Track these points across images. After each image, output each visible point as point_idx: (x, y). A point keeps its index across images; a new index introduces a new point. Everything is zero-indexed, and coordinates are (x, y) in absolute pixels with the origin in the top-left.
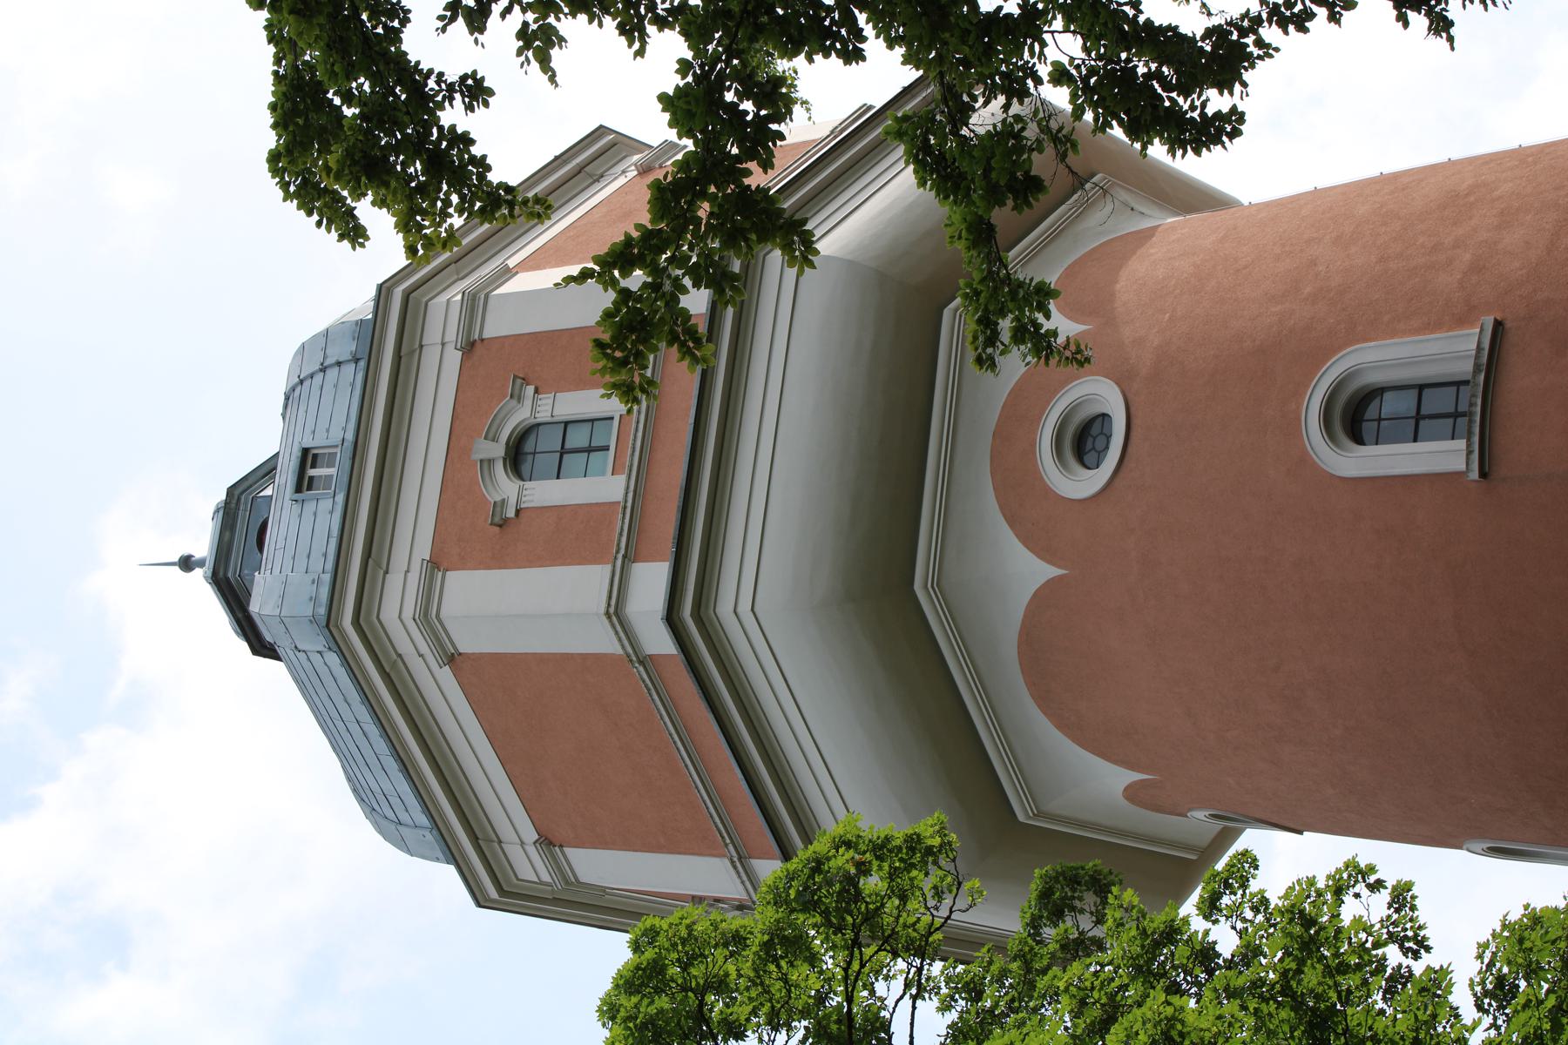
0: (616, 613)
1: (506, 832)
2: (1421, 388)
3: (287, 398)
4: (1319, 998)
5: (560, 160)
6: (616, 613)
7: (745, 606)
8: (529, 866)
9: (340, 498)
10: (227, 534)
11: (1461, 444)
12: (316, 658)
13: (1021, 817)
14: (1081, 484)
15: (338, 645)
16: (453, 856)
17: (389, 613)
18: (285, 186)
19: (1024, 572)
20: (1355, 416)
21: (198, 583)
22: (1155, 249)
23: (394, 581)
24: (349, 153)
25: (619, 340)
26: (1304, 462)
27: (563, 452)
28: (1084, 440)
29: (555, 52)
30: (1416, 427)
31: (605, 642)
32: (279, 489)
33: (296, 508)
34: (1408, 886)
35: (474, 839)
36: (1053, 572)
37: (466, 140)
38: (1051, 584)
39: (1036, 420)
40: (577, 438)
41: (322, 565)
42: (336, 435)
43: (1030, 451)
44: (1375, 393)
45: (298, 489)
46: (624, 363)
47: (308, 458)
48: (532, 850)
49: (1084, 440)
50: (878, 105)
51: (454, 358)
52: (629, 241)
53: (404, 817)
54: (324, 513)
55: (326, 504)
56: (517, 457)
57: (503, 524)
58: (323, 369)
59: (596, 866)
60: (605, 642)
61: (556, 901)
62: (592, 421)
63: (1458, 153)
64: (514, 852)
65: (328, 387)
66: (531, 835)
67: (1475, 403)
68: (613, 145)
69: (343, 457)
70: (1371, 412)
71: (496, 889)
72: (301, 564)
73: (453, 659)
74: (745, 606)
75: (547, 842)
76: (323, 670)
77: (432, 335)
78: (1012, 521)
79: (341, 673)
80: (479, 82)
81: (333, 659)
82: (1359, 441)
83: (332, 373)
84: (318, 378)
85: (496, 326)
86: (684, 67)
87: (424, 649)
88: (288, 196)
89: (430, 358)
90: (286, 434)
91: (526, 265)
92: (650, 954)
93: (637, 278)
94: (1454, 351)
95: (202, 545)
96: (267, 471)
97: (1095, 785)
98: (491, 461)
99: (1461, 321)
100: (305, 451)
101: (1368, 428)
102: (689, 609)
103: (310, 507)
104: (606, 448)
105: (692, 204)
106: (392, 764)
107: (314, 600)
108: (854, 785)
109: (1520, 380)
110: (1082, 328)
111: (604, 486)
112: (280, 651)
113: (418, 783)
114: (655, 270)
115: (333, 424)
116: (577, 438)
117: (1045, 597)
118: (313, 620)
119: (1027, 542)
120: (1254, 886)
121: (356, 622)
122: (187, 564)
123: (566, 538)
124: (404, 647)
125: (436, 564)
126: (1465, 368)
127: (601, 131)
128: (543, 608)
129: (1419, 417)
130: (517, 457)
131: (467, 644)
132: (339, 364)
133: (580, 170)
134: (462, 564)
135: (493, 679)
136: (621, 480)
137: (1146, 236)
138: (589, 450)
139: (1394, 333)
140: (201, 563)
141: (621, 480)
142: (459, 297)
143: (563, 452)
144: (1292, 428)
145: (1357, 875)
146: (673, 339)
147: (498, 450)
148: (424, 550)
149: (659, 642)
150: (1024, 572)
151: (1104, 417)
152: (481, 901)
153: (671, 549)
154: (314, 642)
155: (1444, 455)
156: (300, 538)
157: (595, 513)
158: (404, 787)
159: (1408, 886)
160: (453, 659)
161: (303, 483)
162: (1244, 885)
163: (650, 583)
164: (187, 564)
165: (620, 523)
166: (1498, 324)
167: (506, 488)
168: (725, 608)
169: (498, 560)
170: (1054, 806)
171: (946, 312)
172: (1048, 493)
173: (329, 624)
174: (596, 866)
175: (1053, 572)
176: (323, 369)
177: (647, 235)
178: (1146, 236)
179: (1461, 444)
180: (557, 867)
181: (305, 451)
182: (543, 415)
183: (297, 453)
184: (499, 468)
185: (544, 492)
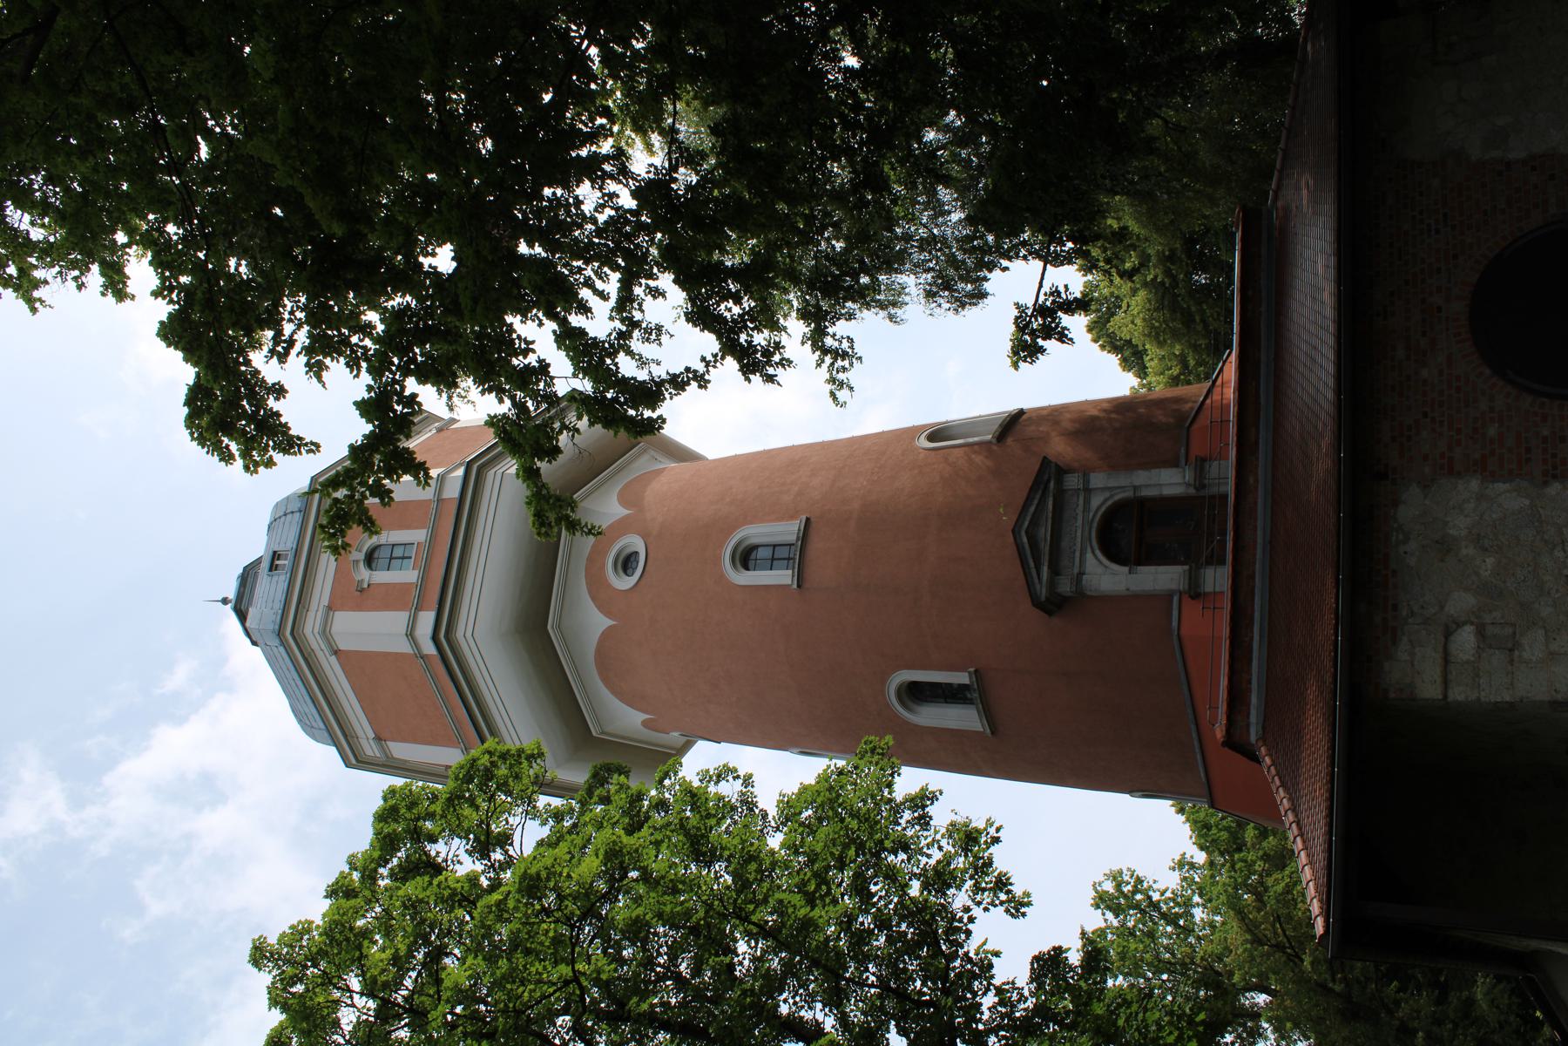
0: (411, 634)
1: (360, 733)
2: (774, 546)
4: (699, 829)
8: (370, 749)
11: (790, 572)
14: (624, 583)
15: (283, 643)
17: (308, 630)
18: (192, 434)
19: (595, 622)
20: (745, 557)
22: (663, 478)
23: (311, 614)
24: (213, 419)
25: (331, 523)
26: (722, 577)
27: (391, 558)
28: (627, 563)
29: (324, 374)
30: (772, 563)
31: (405, 647)
34: (750, 776)
35: (345, 736)
36: (611, 623)
37: (278, 415)
39: (605, 553)
40: (398, 552)
41: (278, 606)
43: (604, 565)
44: (755, 547)
46: (334, 535)
47: (276, 555)
49: (627, 563)
52: (338, 474)
54: (281, 580)
55: (283, 578)
56: (370, 560)
57: (362, 590)
59: (401, 750)
60: (405, 647)
63: (1045, 404)
64: (364, 742)
67: (797, 554)
69: (291, 556)
70: (753, 556)
73: (336, 652)
75: (379, 739)
78: (593, 599)
80: (282, 387)
81: (282, 649)
82: (747, 569)
86: (370, 388)
88: (193, 439)
90: (268, 545)
92: (392, 802)
93: (341, 493)
94: (788, 530)
95: (232, 595)
97: (627, 719)
99: (792, 517)
101: (751, 564)
102: (444, 634)
105: (371, 456)
106: (307, 698)
108: (519, 720)
109: (816, 545)
111: (407, 575)
113: (322, 712)
114: (352, 489)
115: (287, 543)
116: (398, 552)
117: (607, 635)
120: (681, 775)
122: (225, 601)
123: (389, 598)
124: (315, 646)
125: (330, 608)
126: (792, 538)
128: (379, 631)
129: (773, 559)
134: (342, 609)
135: (356, 663)
136: (416, 572)
137: (660, 472)
139: (762, 521)
141: (416, 572)
142: (460, 472)
143: (391, 558)
144: (717, 560)
145: (724, 773)
146: (360, 522)
147: (361, 556)
149: (429, 649)
150: (595, 622)
151: (636, 553)
155: (782, 576)
156: (270, 591)
157: (403, 588)
158: (314, 711)
159: (750, 776)
160: (336, 652)
161: (273, 567)
162: (676, 774)
163: (427, 619)
164: (225, 601)
165: (415, 593)
166: (808, 519)
167: (364, 574)
168: (459, 634)
169: (359, 607)
170: (608, 729)
172: (609, 586)
173: (280, 633)
174: (401, 750)
175: (611, 623)
177: (347, 470)
178: (660, 472)
179: (790, 572)
180: (383, 749)
184: (361, 565)
185: (381, 577)
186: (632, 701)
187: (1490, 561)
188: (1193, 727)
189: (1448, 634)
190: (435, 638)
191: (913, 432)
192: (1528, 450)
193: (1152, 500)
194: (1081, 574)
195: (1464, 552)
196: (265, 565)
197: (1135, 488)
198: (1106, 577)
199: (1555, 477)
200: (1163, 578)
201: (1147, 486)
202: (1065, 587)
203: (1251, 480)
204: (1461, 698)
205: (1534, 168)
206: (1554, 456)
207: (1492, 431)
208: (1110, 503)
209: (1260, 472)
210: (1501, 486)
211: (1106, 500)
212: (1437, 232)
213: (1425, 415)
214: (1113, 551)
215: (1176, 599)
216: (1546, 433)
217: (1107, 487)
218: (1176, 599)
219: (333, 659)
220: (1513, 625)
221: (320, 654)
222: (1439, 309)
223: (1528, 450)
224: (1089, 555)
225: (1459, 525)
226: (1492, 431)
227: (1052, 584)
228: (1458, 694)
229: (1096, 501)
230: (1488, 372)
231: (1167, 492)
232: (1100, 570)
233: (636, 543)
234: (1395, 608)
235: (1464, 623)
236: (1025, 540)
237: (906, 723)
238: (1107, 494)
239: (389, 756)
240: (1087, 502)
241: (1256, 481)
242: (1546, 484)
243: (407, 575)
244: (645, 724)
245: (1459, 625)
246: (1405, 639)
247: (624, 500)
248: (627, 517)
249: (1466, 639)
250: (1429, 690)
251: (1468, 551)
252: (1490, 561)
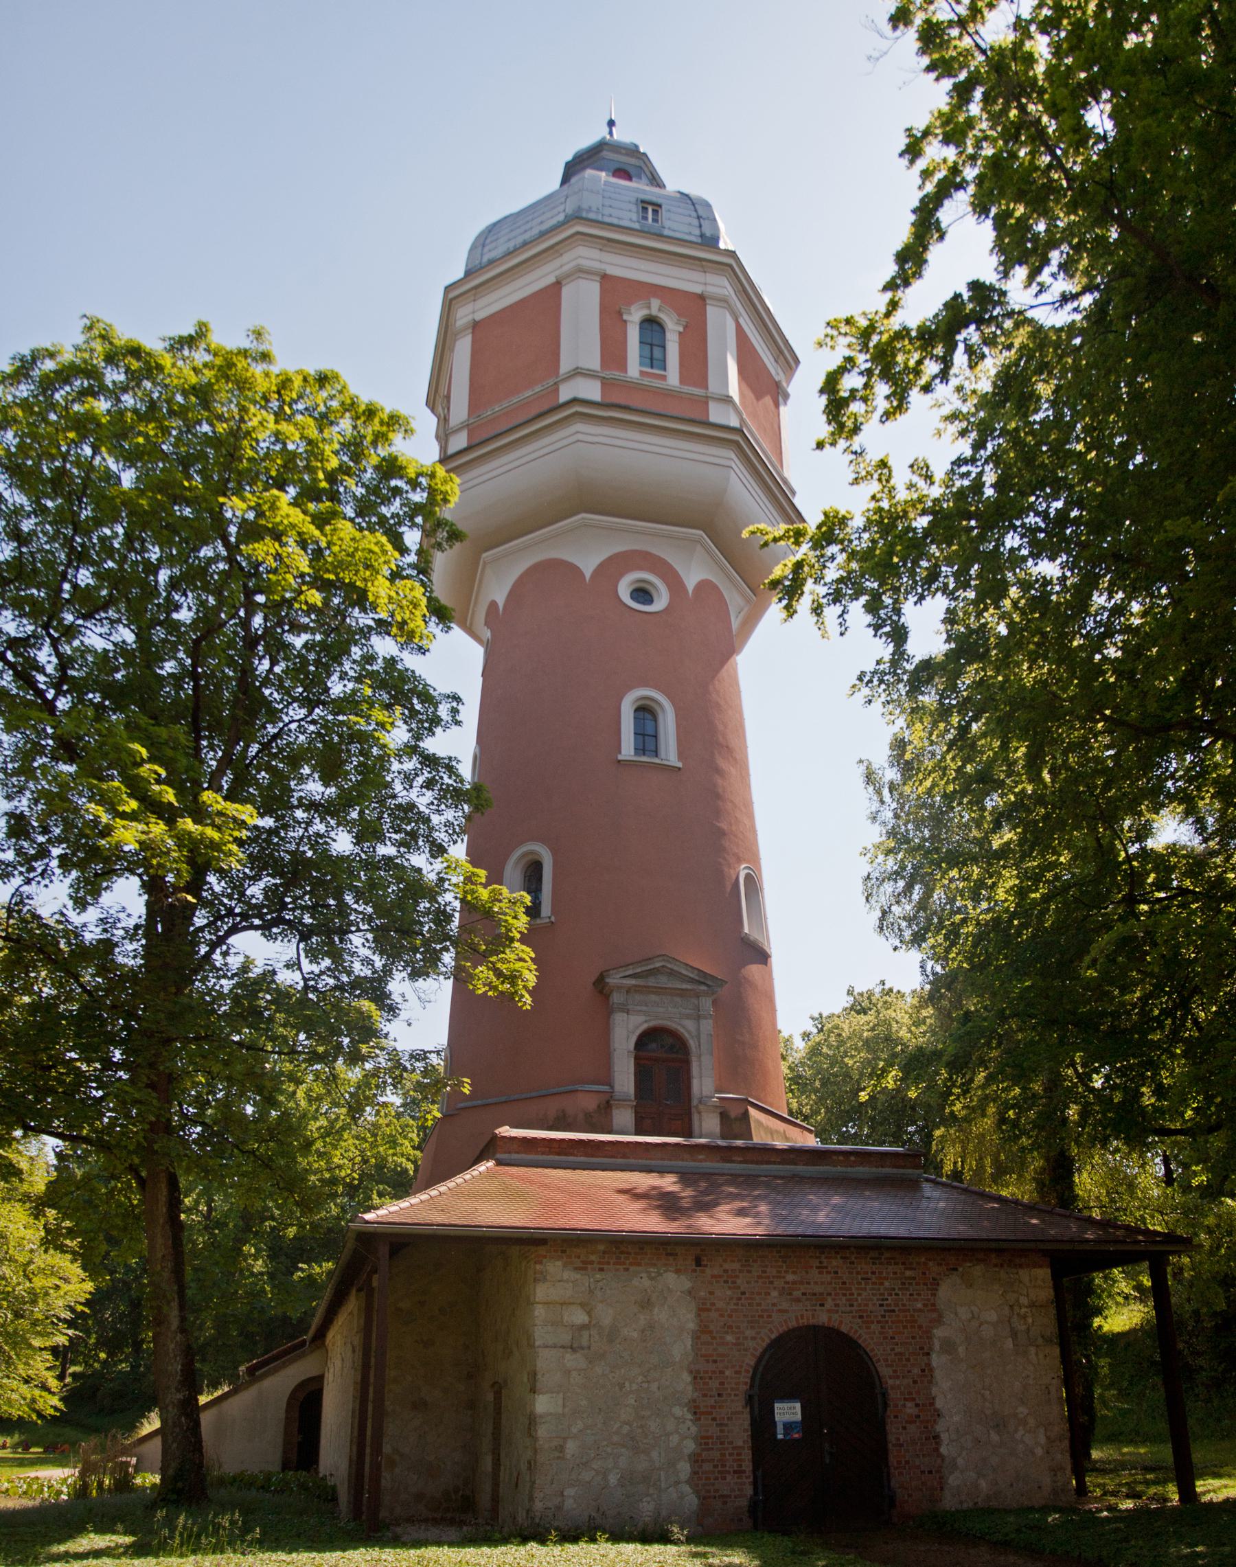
0: (578, 373)
1: (481, 303)
2: (656, 736)
3: (687, 195)
5: (786, 342)
6: (578, 373)
7: (580, 437)
9: (637, 226)
10: (121, 1550)
12: (562, 207)
13: (484, 555)
14: (624, 591)
16: (469, 273)
19: (588, 564)
20: (645, 711)
21: (601, 133)
28: (643, 594)
32: (640, 187)
33: (633, 200)
38: (582, 574)
42: (667, 224)
43: (641, 569)
44: (655, 719)
45: (643, 201)
48: (470, 317)
49: (643, 594)
50: (796, 501)
51: (697, 289)
53: (486, 249)
55: (634, 217)
58: (699, 217)
60: (565, 367)
61: (446, 332)
62: (665, 361)
63: (752, 771)
65: (689, 220)
66: (480, 316)
68: (791, 368)
70: (648, 716)
71: (453, 298)
72: (607, 202)
73: (558, 284)
74: (580, 437)
75: (476, 326)
76: (555, 211)
77: (711, 278)
79: (553, 222)
81: (561, 217)
82: (636, 710)
83: (696, 222)
84: (694, 214)
85: (712, 312)
87: (566, 268)
89: (697, 276)
91: (739, 329)
96: (655, 180)
98: (649, 308)
100: (660, 206)
101: (641, 714)
102: (579, 409)
103: (634, 208)
104: (652, 367)
106: (511, 245)
107: (589, 210)
110: (690, 592)
112: (566, 187)
116: (657, 352)
118: (580, 209)
119: (601, 565)
121: (578, 233)
123: (613, 353)
124: (567, 257)
125: (605, 278)
127: (797, 362)
128: (580, 343)
129: (644, 735)
130: (651, 324)
131: (566, 291)
132: (700, 226)
133: (781, 352)
138: (652, 359)
140: (611, 133)
142: (734, 422)
143: (651, 345)
144: (645, 684)
147: (654, 312)
148: (611, 271)
149: (565, 394)
150: (588, 564)
152: (448, 289)
153: (608, 401)
154: (570, 207)
157: (622, 365)
161: (644, 204)
163: (591, 390)
165: (617, 374)
168: (580, 427)
171: (701, 532)
172: (621, 575)
176: (699, 217)
180: (464, 329)
181: (660, 206)
182: (669, 336)
183: (659, 201)
186: (515, 595)
187: (635, 1335)
188: (503, 1099)
189: (582, 1305)
190: (575, 401)
191: (755, 859)
192: (715, 1361)
193: (688, 1071)
194: (628, 1012)
195: (642, 1317)
196: (650, 192)
197: (700, 1056)
198: (625, 1031)
199: (695, 1378)
200: (625, 1079)
201: (700, 1066)
202: (617, 998)
203: (701, 1157)
204: (536, 1313)
205: (923, 1371)
206: (711, 1378)
207: (729, 1338)
208: (687, 1035)
209: (708, 1164)
210: (689, 1343)
211: (689, 1032)
212: (881, 1305)
213: (743, 1293)
214: (646, 1039)
215: (606, 1088)
216: (727, 1373)
217: (701, 1034)
218: (606, 1088)
219: (551, 279)
220: (589, 1348)
221: (557, 263)
222: (822, 1305)
223: (715, 1361)
224: (643, 1018)
225: (660, 1314)
226: (729, 1338)
227: (619, 988)
228: (539, 1312)
229: (690, 1024)
230: (773, 1337)
231: (695, 1083)
232: (631, 1026)
233: (660, 604)
234: (601, 1270)
235: (590, 1316)
236: (658, 965)
237: (507, 857)
238: (694, 1033)
239: (457, 335)
240: (688, 1017)
241: (701, 1161)
242: (691, 1372)
243: (634, 368)
244: (493, 604)
245: (589, 1313)
246: (578, 1276)
247: (703, 586)
248: (685, 590)
249: (580, 1317)
250: (541, 1292)
251: (642, 1320)
252: (635, 1335)
